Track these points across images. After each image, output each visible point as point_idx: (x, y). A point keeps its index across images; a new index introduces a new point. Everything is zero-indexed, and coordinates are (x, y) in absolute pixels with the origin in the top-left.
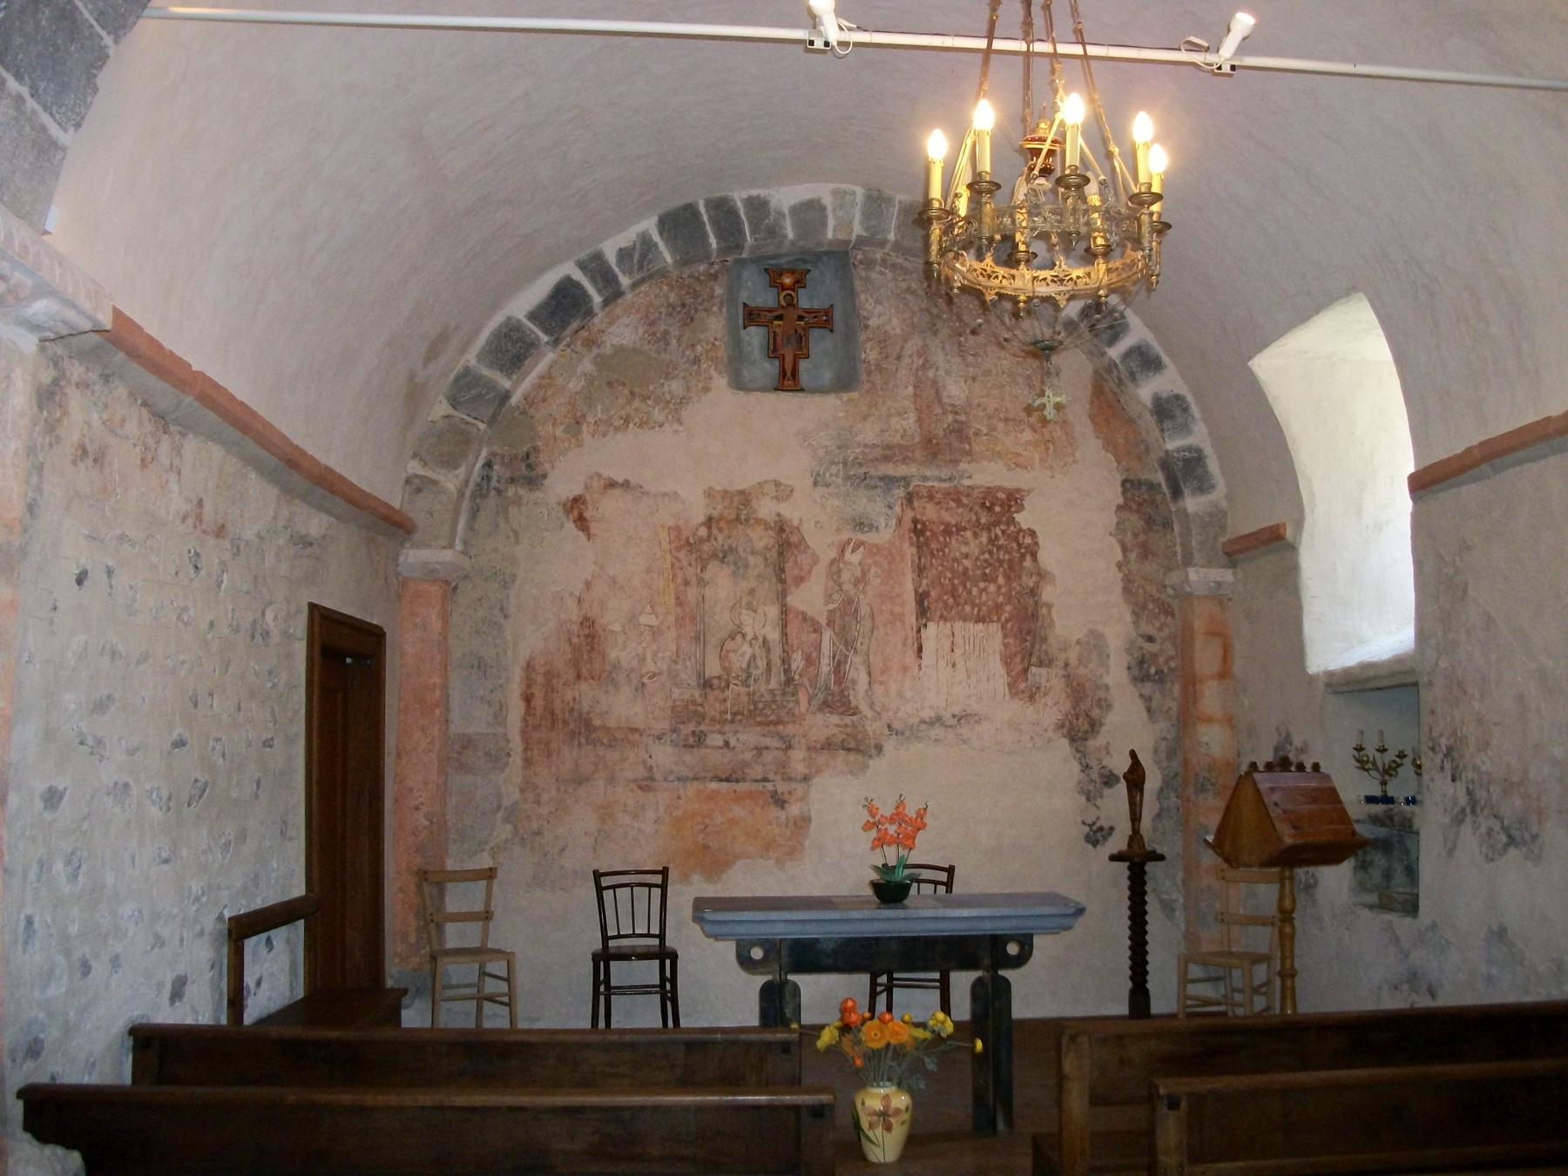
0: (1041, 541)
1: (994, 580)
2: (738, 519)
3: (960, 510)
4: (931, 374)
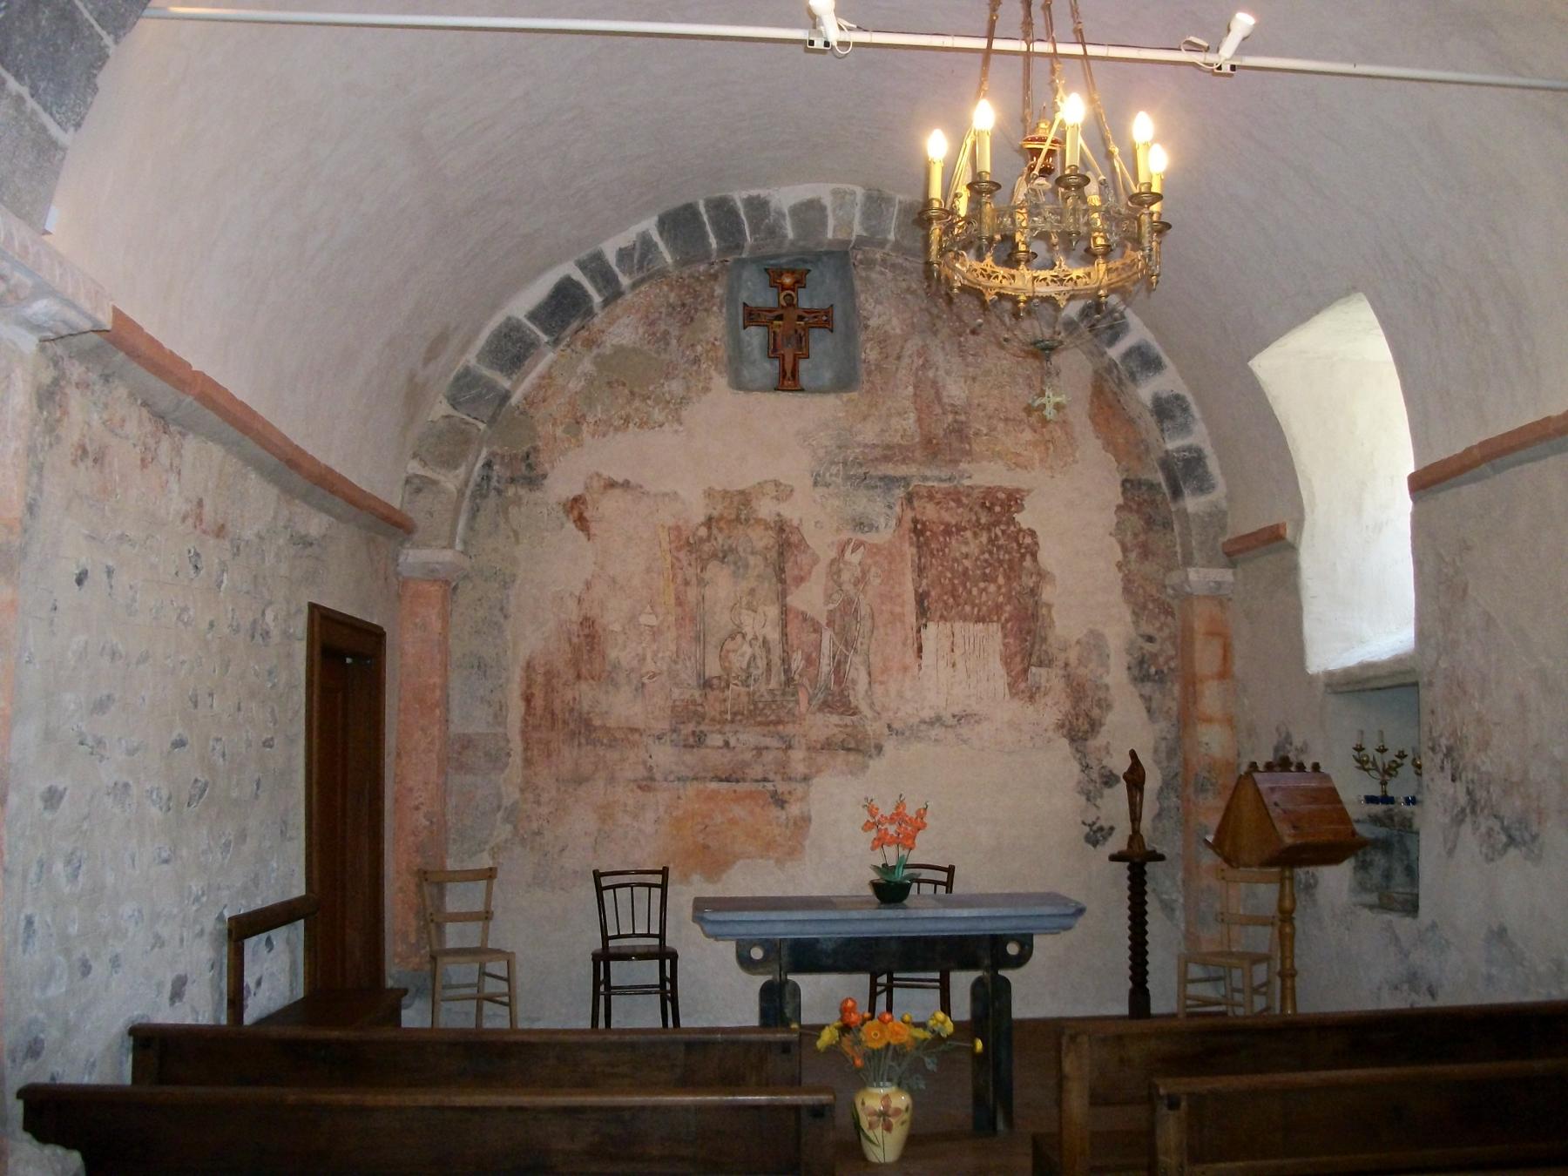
0: (1041, 541)
1: (994, 580)
2: (738, 519)
3: (960, 510)
4: (931, 374)
